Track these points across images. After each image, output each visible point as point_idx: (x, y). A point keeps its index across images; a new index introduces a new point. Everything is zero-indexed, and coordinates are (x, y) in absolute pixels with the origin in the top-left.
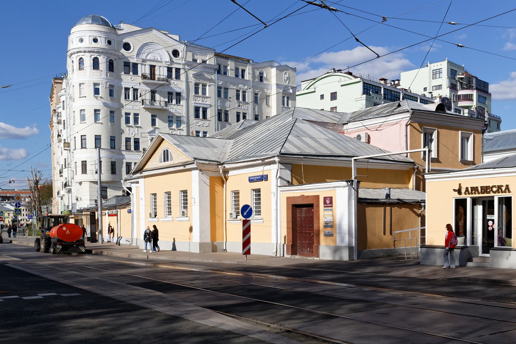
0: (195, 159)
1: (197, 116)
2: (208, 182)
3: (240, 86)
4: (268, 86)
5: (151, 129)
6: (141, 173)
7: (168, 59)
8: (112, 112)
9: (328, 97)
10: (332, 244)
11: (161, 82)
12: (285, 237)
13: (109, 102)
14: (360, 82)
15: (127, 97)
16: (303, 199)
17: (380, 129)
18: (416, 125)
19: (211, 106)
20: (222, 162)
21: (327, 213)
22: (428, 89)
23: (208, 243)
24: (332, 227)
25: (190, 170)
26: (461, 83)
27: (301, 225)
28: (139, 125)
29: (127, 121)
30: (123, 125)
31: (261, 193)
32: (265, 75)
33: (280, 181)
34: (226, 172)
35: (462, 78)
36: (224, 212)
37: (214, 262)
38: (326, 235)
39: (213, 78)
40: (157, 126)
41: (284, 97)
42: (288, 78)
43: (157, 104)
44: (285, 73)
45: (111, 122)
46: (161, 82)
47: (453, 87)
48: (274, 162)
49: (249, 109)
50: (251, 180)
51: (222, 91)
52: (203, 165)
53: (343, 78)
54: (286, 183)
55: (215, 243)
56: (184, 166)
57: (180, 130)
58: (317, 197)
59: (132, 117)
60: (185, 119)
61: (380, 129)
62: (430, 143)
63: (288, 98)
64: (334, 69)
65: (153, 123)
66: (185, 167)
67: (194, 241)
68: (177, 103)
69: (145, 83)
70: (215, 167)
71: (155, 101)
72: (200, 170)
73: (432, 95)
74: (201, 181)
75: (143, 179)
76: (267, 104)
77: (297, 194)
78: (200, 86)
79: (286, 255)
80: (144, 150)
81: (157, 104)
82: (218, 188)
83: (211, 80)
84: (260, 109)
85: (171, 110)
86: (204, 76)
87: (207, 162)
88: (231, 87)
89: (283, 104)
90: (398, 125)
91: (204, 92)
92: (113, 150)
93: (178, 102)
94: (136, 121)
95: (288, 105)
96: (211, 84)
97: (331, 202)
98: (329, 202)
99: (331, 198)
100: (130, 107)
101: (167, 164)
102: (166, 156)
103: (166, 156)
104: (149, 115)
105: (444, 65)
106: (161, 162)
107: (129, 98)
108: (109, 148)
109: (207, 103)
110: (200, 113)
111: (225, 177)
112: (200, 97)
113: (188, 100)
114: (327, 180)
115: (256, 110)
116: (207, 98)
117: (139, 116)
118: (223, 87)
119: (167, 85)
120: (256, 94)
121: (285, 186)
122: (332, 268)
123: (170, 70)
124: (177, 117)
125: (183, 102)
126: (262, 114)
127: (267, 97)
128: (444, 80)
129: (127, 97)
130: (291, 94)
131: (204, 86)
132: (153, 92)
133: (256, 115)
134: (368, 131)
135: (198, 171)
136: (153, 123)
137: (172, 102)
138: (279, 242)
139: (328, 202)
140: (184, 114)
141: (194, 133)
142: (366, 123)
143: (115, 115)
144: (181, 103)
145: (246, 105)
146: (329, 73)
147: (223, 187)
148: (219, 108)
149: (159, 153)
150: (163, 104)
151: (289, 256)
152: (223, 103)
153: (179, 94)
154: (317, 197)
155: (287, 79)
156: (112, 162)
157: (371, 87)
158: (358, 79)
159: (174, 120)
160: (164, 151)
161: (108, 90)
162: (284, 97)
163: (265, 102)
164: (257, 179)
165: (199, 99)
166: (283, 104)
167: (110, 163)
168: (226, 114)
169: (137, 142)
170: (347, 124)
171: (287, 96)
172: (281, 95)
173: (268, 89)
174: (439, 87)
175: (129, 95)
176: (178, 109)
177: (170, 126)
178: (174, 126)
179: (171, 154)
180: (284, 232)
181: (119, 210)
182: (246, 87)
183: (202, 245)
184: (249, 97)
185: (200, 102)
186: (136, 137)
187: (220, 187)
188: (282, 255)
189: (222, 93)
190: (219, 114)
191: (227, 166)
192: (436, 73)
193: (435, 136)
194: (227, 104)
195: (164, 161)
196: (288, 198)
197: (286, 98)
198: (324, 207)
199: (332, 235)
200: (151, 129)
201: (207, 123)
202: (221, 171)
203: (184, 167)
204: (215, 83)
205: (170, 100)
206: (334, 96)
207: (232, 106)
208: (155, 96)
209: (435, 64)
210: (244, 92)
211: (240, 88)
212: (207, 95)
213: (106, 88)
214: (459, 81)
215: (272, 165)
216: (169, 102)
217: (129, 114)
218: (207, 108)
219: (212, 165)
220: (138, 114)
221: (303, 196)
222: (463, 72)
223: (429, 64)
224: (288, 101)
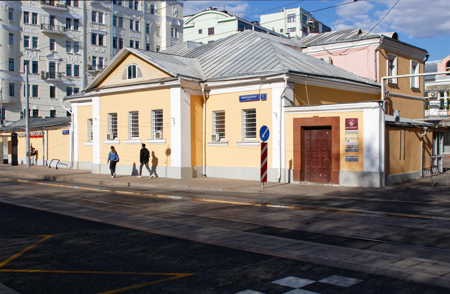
0: (179, 75)
1: (94, 42)
2: (189, 100)
3: (134, 16)
4: (159, 18)
5: (50, 52)
6: (98, 90)
8: (11, 35)
9: (205, 32)
10: (358, 169)
11: (60, 8)
12: (291, 162)
13: (9, 25)
14: (236, 19)
15: (26, 21)
16: (317, 120)
17: (345, 53)
18: (383, 51)
19: (107, 33)
20: (204, 80)
21: (349, 136)
22: (284, 30)
23: (190, 168)
24: (356, 151)
25: (169, 87)
26: (310, 27)
27: (311, 149)
28: (38, 48)
29: (26, 44)
30: (22, 48)
31: (118, 117)
32: (156, 8)
33: (285, 101)
34: (207, 90)
35: (311, 23)
36: (204, 134)
37: (225, 191)
38: (349, 160)
39: (109, 7)
40: (55, 50)
41: (172, 29)
42: (177, 12)
43: (56, 29)
44: (174, 8)
45: (10, 44)
46: (60, 8)
47: (304, 30)
48: (282, 80)
49: (142, 39)
50: (242, 99)
51: (117, 20)
52: (186, 82)
53: (219, 16)
54: (289, 103)
55: (195, 168)
56: (162, 83)
57: (78, 55)
58: (337, 119)
59: (30, 41)
60: (82, 45)
61: (345, 53)
62: (390, 69)
63: (176, 30)
64: (211, 8)
65: (52, 47)
66: (161, 84)
67: (172, 165)
68: (75, 29)
69: (43, 8)
70: (197, 84)
71: (53, 26)
72: (182, 88)
73: (289, 36)
74: (183, 100)
75: (98, 97)
76: (158, 35)
77: (310, 115)
78: (97, 14)
79: (292, 181)
80: (43, 73)
81: (56, 29)
82: (198, 107)
83: (107, 9)
84: (152, 39)
85: (69, 36)
86: (101, 5)
87: (190, 79)
88: (126, 16)
89: (172, 35)
90: (366, 51)
91: (101, 21)
92: (12, 72)
93: (76, 28)
94: (35, 44)
95: (176, 36)
96: (107, 12)
97: (356, 124)
98: (353, 124)
99: (356, 120)
100: (28, 30)
102: (132, 72)
103: (132, 72)
104: (47, 39)
105: (297, 11)
106: (124, 78)
107: (28, 22)
108: (8, 70)
109: (103, 30)
110: (97, 39)
111: (206, 96)
112: (97, 24)
113: (85, 27)
114: (322, 102)
115: (148, 39)
116: (103, 25)
117: (38, 40)
118: (118, 16)
119: (66, 11)
120: (148, 25)
121: (288, 106)
122: (358, 198)
124: (75, 42)
125: (81, 29)
126: (153, 43)
127: (158, 28)
128: (297, 24)
129: (26, 21)
130: (179, 26)
131: (101, 14)
132: (52, 18)
133: (147, 44)
134: (330, 56)
135: (179, 89)
136: (52, 47)
137: (70, 28)
138: (283, 167)
139: (351, 124)
140: (82, 39)
141: (91, 58)
142: (328, 47)
143: (14, 37)
144: (79, 29)
145: (139, 35)
146: (207, 10)
147: (202, 107)
148: (115, 36)
150: (61, 29)
151: (298, 183)
152: (118, 32)
153: (76, 21)
154: (337, 119)
155: (176, 13)
156: (10, 84)
157: (244, 25)
158: (234, 18)
159: (72, 45)
160: (130, 68)
161: (8, 12)
162: (172, 29)
163: (156, 32)
164: (252, 99)
165: (95, 26)
166: (172, 35)
167: (8, 85)
168: (121, 42)
169: (35, 65)
170: (306, 47)
171: (176, 28)
172: (170, 27)
173: (158, 21)
174: (293, 29)
175: (28, 19)
176: (77, 35)
177: (68, 51)
178: (72, 51)
179: (139, 69)
180: (291, 156)
181: (45, 132)
182: (139, 18)
183: (183, 170)
184: (142, 27)
185: (97, 29)
186: (35, 60)
187: (200, 107)
188: (287, 182)
189: (117, 21)
190: (114, 41)
191: (210, 84)
192: (291, 18)
193: (395, 63)
194: (122, 32)
195: (130, 77)
196: (295, 120)
197: (174, 29)
198: (346, 129)
199: (356, 160)
200: (50, 52)
201: (103, 49)
202: (203, 90)
203: (161, 85)
204: (111, 12)
205: (68, 26)
206: (211, 31)
207: (127, 35)
208: (53, 21)
209: (290, 10)
210: (137, 22)
211: (134, 18)
212: (104, 23)
213: (5, 10)
214: (309, 26)
215: (273, 84)
216: (67, 27)
217: (28, 37)
218: (103, 35)
219: (195, 82)
220: (37, 38)
221: (316, 118)
222: (311, 18)
223: (284, 10)
224: (176, 32)
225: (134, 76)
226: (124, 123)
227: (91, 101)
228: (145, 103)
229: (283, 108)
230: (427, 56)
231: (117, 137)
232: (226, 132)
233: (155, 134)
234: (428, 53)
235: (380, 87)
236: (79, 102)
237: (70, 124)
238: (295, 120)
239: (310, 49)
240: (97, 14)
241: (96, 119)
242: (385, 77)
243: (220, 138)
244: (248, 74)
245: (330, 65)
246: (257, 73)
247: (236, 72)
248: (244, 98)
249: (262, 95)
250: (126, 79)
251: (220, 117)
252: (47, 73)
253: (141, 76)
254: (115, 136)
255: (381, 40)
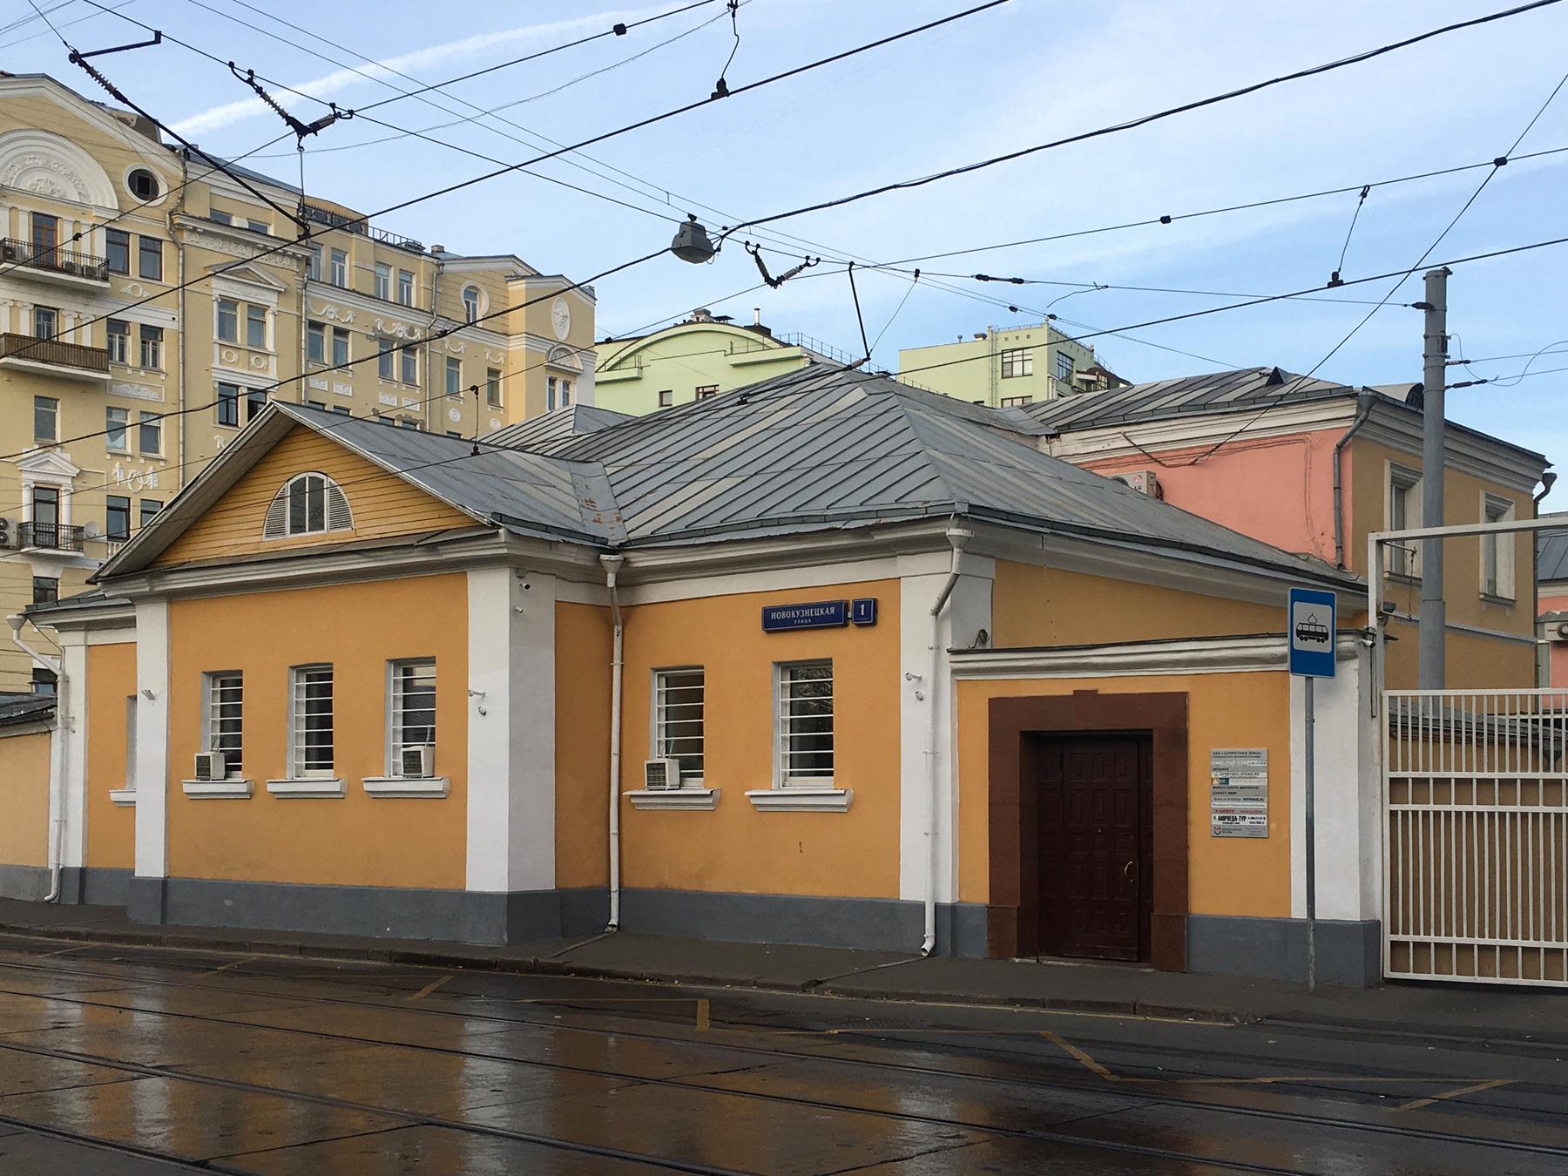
7: (111, 202)
31: (246, 688)
34: (631, 579)
48: (939, 544)
50: (777, 621)
78: (241, 313)
101: (309, 538)
103: (307, 507)
123: (117, 240)
131: (257, 311)
134: (1154, 467)
149: (277, 484)
164: (815, 620)
165: (235, 357)
179: (336, 496)
191: (642, 561)
196: (996, 705)
221: (1085, 698)
225: (317, 524)
226: (274, 710)
227: (131, 623)
228: (358, 637)
229: (947, 657)
230: (1549, 480)
231: (239, 768)
232: (708, 754)
233: (400, 760)
234: (1549, 465)
235: (1365, 589)
236: (89, 627)
237: (52, 716)
238: (996, 705)
239: (1071, 444)
240: (241, 313)
241: (150, 696)
242: (1385, 535)
243: (682, 776)
244: (803, 520)
245: (1154, 501)
246: (837, 517)
247: (751, 514)
248: (784, 615)
249: (857, 604)
250: (282, 532)
251: (686, 690)
252: (21, 526)
253: (347, 523)
254: (233, 762)
255: (1359, 407)
